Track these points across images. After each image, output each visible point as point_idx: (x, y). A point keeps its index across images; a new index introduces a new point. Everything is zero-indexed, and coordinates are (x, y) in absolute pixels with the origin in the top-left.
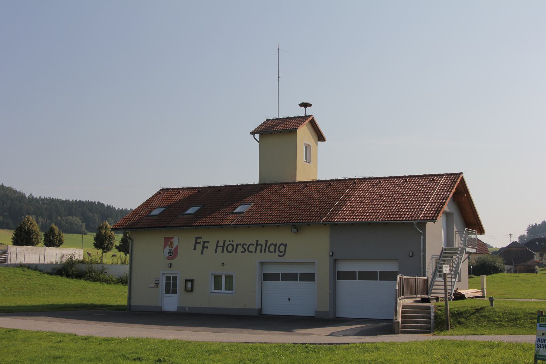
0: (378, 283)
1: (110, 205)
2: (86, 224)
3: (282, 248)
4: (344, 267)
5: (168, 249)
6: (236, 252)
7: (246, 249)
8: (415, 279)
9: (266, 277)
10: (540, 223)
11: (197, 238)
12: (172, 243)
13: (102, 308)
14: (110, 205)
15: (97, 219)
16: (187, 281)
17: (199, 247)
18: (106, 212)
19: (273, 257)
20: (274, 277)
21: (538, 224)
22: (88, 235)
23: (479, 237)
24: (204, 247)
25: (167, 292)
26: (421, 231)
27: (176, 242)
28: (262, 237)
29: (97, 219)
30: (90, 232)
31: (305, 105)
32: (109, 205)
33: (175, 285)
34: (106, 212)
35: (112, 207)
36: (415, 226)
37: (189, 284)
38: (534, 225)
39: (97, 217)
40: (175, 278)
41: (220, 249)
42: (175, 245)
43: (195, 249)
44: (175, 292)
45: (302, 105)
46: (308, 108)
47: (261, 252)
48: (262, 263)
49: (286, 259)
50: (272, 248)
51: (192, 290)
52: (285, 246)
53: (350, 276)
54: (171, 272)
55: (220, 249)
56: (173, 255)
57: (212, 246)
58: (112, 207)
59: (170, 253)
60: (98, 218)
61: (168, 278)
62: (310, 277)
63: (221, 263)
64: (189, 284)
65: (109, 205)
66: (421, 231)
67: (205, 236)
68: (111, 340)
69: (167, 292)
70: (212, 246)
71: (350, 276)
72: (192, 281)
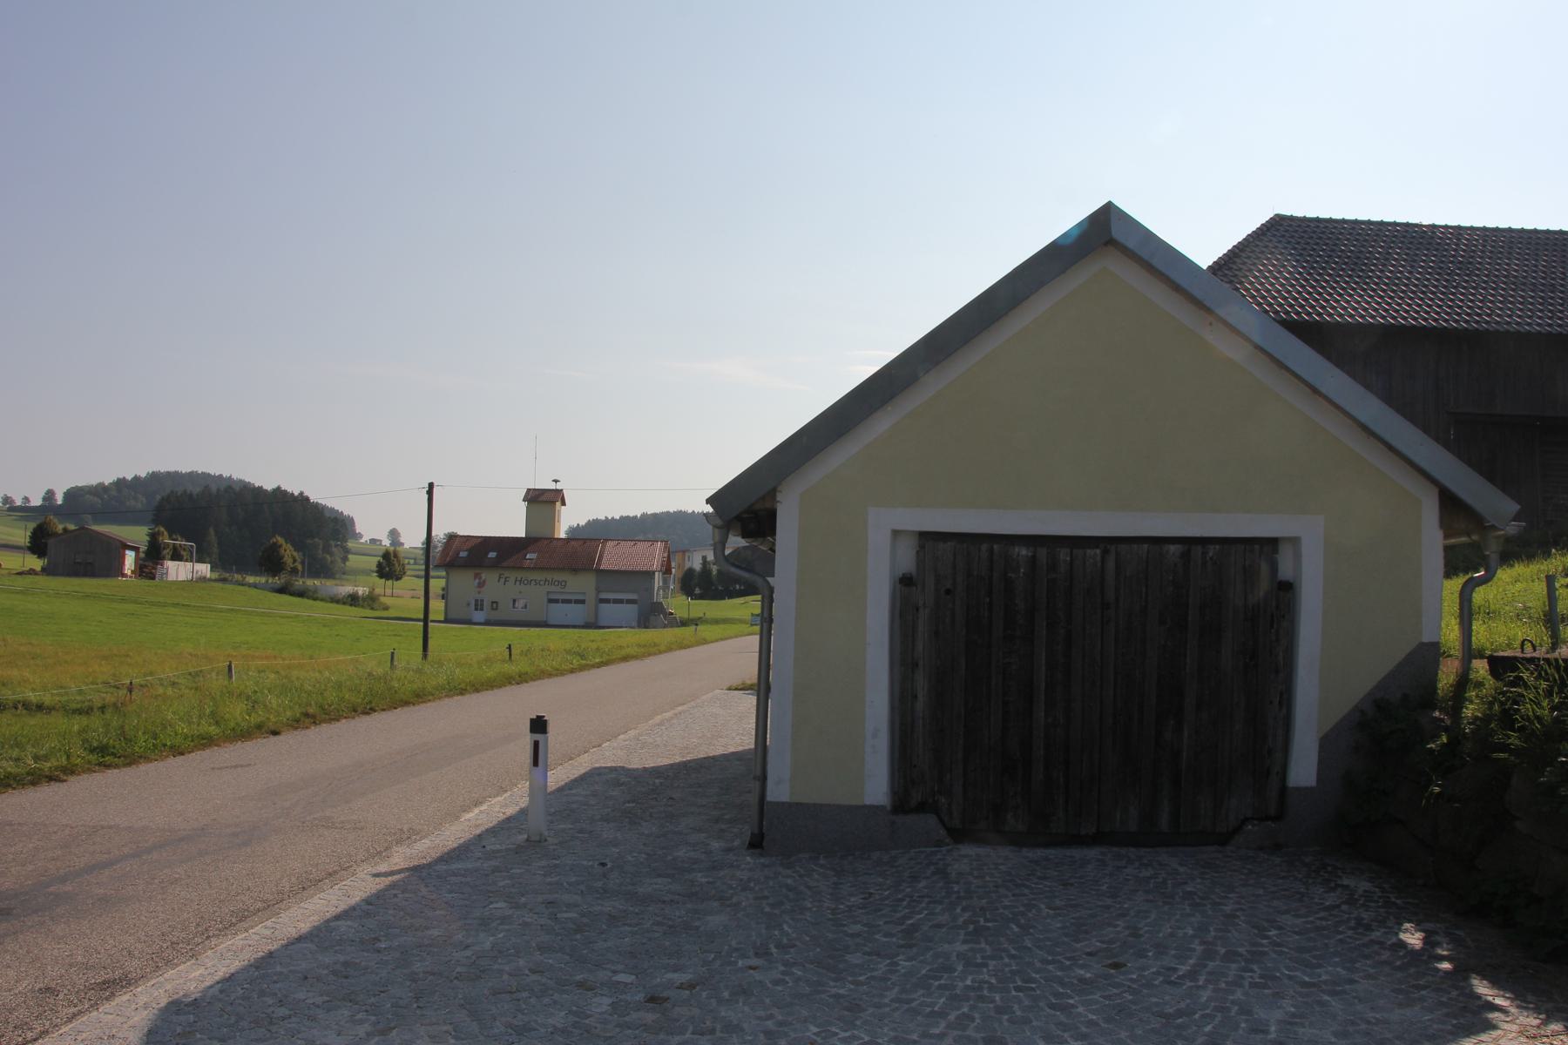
0: (573, 605)
3: (563, 584)
4: (604, 596)
5: (477, 581)
7: (537, 583)
9: (551, 601)
10: (584, 524)
11: (500, 575)
12: (480, 578)
16: (493, 602)
17: (502, 580)
19: (558, 589)
20: (556, 601)
21: (581, 524)
24: (505, 581)
25: (476, 609)
26: (1564, 759)
27: (484, 576)
28: (549, 576)
31: (556, 481)
33: (482, 605)
37: (495, 605)
38: (575, 525)
40: (482, 601)
41: (518, 583)
42: (483, 578)
43: (499, 581)
44: (482, 609)
48: (548, 592)
49: (566, 590)
50: (556, 583)
51: (497, 609)
52: (566, 582)
53: (607, 601)
54: (479, 597)
55: (518, 583)
56: (481, 585)
57: (512, 579)
59: (479, 583)
61: (476, 601)
62: (582, 602)
64: (495, 605)
66: (1564, 759)
67: (507, 574)
69: (476, 609)
70: (512, 579)
71: (607, 601)
72: (496, 602)
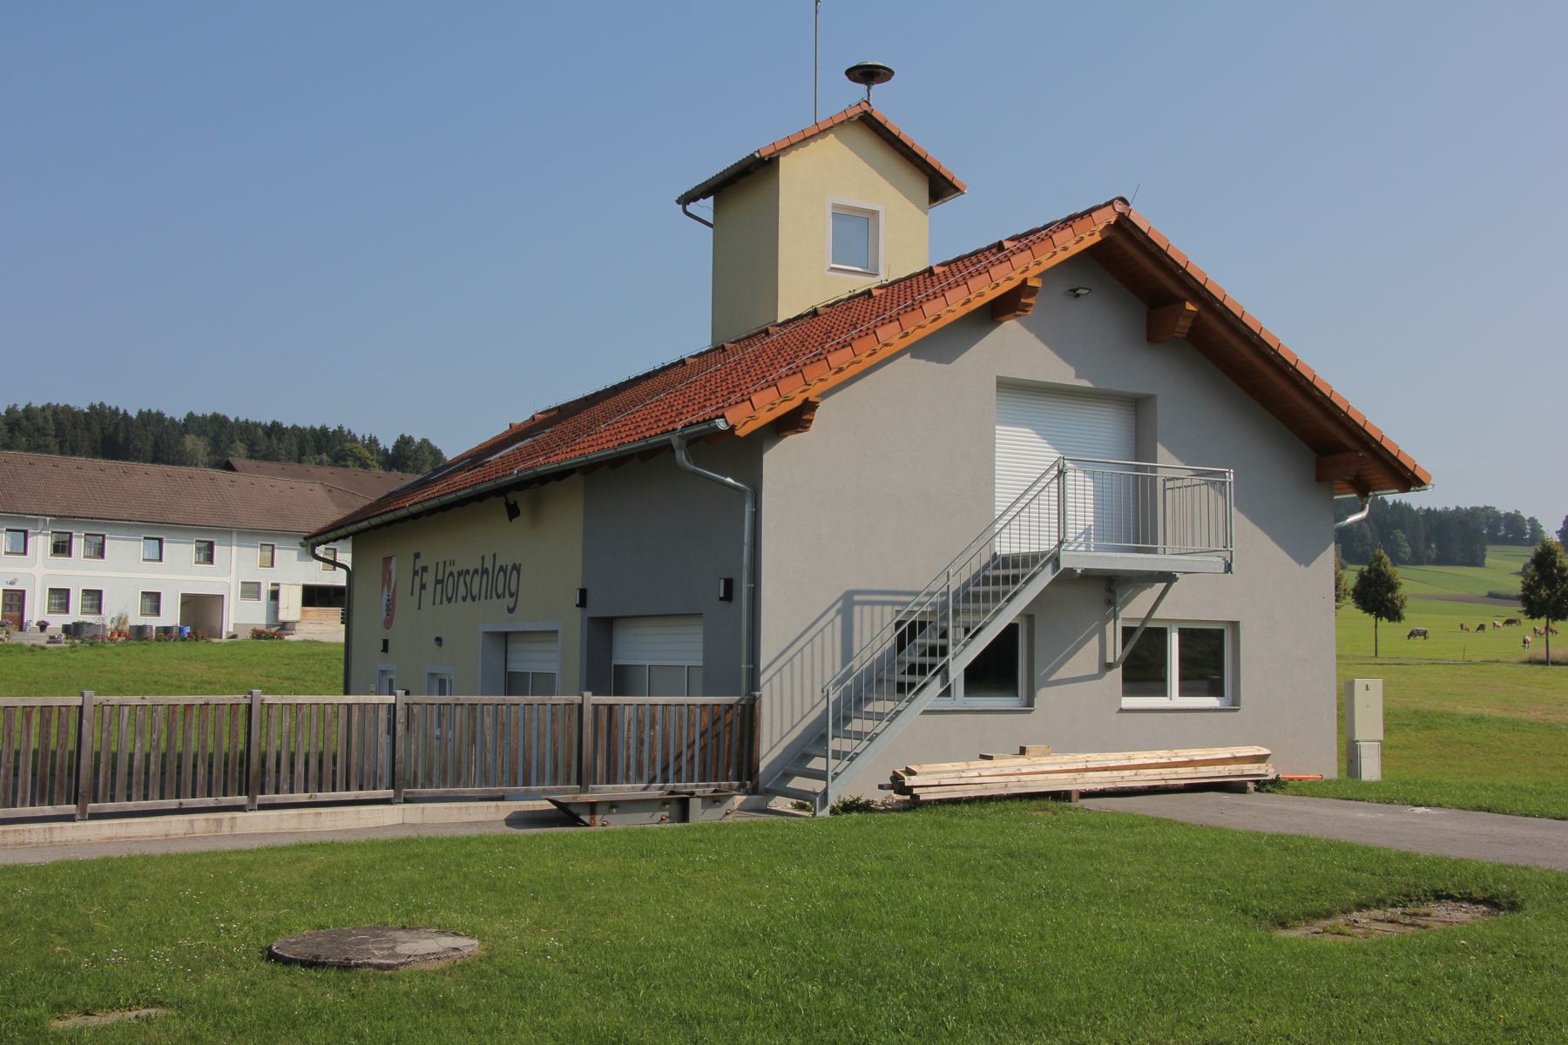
1: (1400, 502)
2: (1343, 547)
6: (456, 601)
8: (581, 706)
13: (48, 790)
14: (1400, 502)
15: (1370, 534)
18: (1388, 516)
22: (1350, 570)
23: (1414, 500)
29: (1370, 534)
30: (1351, 563)
31: (867, 74)
32: (1397, 502)
34: (1388, 516)
35: (1406, 504)
36: (681, 456)
39: (1368, 529)
45: (857, 73)
46: (876, 88)
47: (486, 598)
58: (1406, 504)
60: (1371, 530)
63: (433, 638)
65: (1397, 502)
66: (729, 480)
68: (1170, 823)
